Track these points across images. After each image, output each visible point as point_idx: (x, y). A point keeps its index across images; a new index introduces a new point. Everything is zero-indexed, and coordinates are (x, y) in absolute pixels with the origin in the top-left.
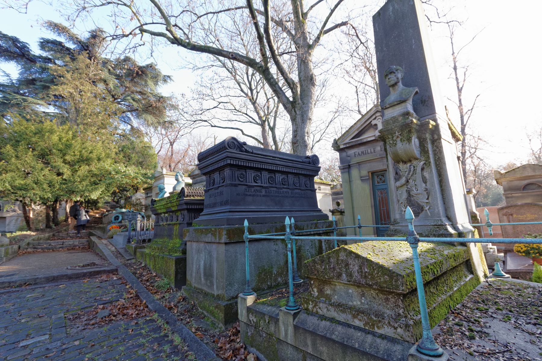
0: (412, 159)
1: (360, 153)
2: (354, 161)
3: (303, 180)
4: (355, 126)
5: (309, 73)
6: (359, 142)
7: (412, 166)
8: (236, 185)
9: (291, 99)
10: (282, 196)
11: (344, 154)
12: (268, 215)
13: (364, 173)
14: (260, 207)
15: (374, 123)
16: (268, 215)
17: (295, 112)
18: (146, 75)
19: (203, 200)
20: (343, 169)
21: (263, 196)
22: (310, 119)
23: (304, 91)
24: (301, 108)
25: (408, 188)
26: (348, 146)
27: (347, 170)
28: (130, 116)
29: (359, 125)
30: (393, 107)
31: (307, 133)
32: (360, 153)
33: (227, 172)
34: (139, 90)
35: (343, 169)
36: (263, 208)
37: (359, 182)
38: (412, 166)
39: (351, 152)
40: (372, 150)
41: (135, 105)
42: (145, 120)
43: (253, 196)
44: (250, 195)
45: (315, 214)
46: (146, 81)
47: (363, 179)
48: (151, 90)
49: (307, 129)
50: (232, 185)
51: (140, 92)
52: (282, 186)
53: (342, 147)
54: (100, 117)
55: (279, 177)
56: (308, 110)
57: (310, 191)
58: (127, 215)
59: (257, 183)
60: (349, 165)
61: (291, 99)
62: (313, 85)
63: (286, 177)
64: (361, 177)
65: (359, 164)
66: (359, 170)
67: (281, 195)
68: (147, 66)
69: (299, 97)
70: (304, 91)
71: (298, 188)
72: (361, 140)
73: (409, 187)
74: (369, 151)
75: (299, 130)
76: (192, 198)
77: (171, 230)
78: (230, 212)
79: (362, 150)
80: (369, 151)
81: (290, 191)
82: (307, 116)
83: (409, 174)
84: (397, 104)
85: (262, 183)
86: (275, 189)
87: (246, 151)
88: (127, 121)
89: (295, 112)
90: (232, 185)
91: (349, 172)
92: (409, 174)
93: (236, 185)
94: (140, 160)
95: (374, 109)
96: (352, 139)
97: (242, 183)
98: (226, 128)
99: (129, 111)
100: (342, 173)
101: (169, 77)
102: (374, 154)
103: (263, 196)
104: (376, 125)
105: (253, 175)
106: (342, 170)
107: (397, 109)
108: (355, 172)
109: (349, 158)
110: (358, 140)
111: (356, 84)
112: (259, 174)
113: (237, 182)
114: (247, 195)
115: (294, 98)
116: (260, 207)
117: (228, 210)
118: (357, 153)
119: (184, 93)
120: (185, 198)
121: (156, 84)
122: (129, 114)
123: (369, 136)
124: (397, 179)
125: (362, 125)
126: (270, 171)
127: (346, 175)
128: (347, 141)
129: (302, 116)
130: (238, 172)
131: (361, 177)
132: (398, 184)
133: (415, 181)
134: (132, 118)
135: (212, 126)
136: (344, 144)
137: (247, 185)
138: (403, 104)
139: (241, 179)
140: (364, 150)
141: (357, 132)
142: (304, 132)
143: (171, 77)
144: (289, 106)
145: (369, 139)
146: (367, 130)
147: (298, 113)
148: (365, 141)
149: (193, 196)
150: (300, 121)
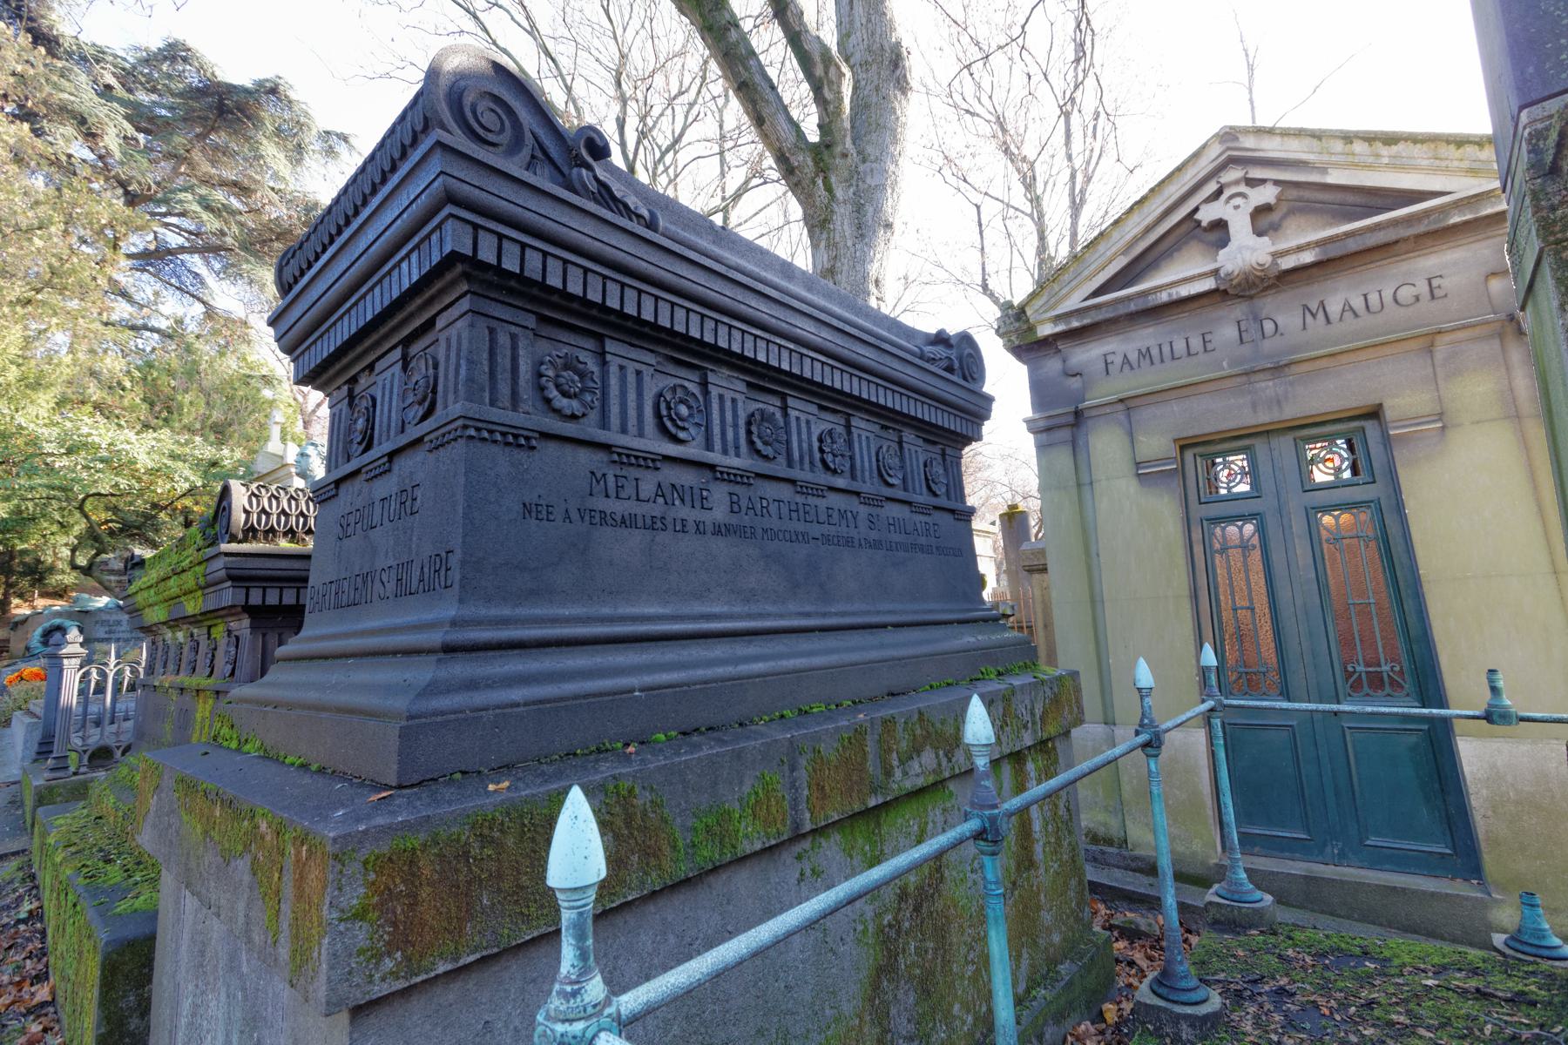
1: (1133, 357)
3: (917, 450)
4: (1116, 235)
5: (885, 35)
6: (1133, 307)
8: (518, 440)
9: (813, 136)
10: (827, 539)
11: (1053, 365)
12: (756, 660)
13: (1156, 444)
14: (698, 608)
16: (756, 660)
17: (829, 189)
18: (257, 122)
19: (307, 557)
20: (1048, 429)
21: (719, 530)
22: (889, 226)
23: (867, 106)
24: (854, 176)
26: (1075, 324)
27: (1065, 434)
28: (202, 270)
29: (1133, 228)
31: (877, 282)
32: (1133, 357)
33: (457, 328)
34: (230, 175)
35: (1048, 429)
36: (722, 611)
39: (1087, 354)
40: (1196, 343)
41: (212, 223)
42: (251, 282)
43: (654, 525)
44: (627, 522)
45: (970, 638)
46: (255, 149)
47: (1145, 473)
48: (276, 176)
49: (876, 265)
50: (480, 432)
51: (235, 184)
52: (824, 478)
53: (1046, 330)
54: (36, 241)
55: (808, 423)
56: (881, 187)
57: (948, 517)
58: (103, 623)
59: (676, 440)
60: (1078, 414)
61: (813, 136)
62: (903, 86)
63: (840, 429)
64: (1138, 465)
65: (1127, 404)
67: (816, 530)
68: (260, 84)
69: (847, 125)
70: (867, 106)
71: (900, 494)
74: (1180, 346)
75: (844, 265)
76: (284, 545)
77: (185, 719)
78: (450, 649)
79: (1143, 345)
80: (1180, 346)
81: (863, 511)
82: (878, 210)
85: (709, 446)
86: (785, 492)
87: (605, 194)
88: (191, 289)
89: (829, 189)
90: (480, 432)
93: (518, 440)
94: (217, 415)
95: (1215, 150)
96: (1097, 293)
97: (569, 429)
99: (192, 250)
101: (344, 138)
102: (1202, 357)
103: (719, 530)
104: (1220, 225)
105: (652, 386)
108: (1106, 444)
109: (1075, 383)
110: (1129, 298)
111: (978, 198)
112: (693, 388)
113: (531, 417)
114: (604, 518)
116: (698, 608)
117: (435, 638)
118: (1118, 360)
120: (225, 547)
121: (297, 153)
122: (195, 262)
123: (1185, 274)
125: (1149, 229)
126: (761, 377)
127: (1063, 458)
128: (1074, 302)
129: (859, 209)
130: (543, 347)
134: (210, 280)
136: (1058, 319)
137: (606, 447)
139: (561, 402)
141: (1122, 262)
142: (865, 278)
143: (351, 140)
144: (803, 160)
145: (1185, 291)
147: (839, 193)
148: (1164, 297)
149: (291, 533)
150: (848, 231)
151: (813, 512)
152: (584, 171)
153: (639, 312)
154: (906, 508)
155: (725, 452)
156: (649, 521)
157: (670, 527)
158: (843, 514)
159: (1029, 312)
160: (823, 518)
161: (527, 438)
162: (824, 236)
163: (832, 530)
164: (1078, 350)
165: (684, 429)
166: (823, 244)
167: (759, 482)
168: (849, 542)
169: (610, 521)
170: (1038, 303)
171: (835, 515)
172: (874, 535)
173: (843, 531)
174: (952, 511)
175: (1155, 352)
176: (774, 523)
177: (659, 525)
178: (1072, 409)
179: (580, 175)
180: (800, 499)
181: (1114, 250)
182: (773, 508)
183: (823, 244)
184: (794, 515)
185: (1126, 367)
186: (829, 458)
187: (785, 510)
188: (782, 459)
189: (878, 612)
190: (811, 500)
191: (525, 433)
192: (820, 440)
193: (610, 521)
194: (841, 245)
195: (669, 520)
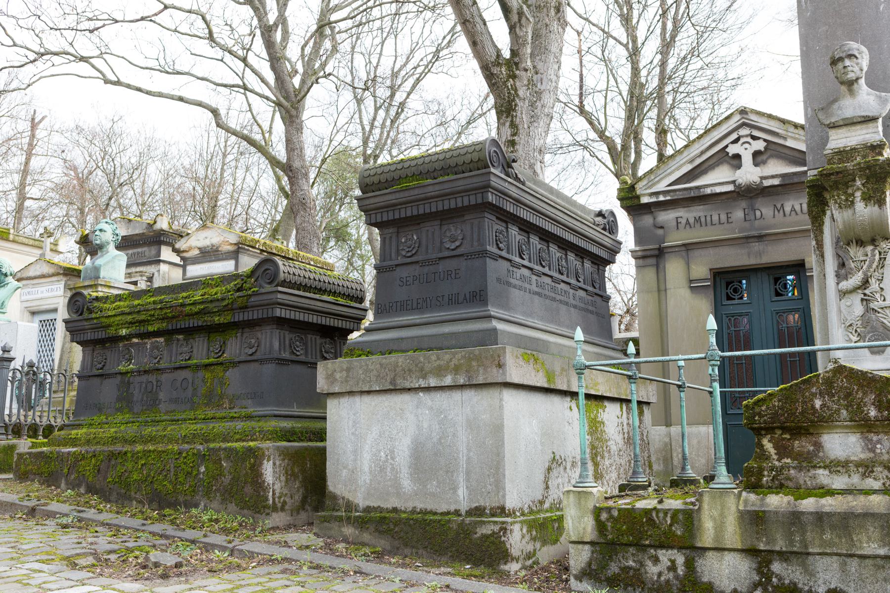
0: (878, 237)
1: (692, 221)
2: (674, 239)
7: (877, 251)
10: (561, 301)
11: (647, 220)
13: (701, 270)
15: (732, 150)
20: (644, 257)
25: (865, 295)
27: (653, 261)
30: (849, 128)
32: (692, 221)
37: (685, 292)
38: (877, 251)
39: (667, 217)
40: (723, 217)
47: (694, 287)
53: (645, 200)
64: (691, 281)
65: (688, 247)
66: (688, 264)
72: (698, 188)
73: (867, 292)
74: (715, 218)
79: (697, 214)
80: (715, 218)
83: (870, 266)
84: (859, 122)
91: (659, 268)
92: (870, 266)
98: (160, 95)
100: (638, 267)
102: (726, 226)
106: (641, 261)
107: (859, 132)
108: (674, 269)
110: (691, 189)
115: (514, 53)
118: (684, 221)
119: (828, 60)
124: (839, 277)
125: (702, 153)
127: (651, 273)
128: (662, 186)
131: (691, 281)
132: (845, 285)
133: (881, 280)
135: (107, 81)
138: (871, 125)
140: (702, 214)
141: (689, 167)
145: (718, 189)
146: (712, 167)
148: (708, 191)
158: (565, 292)
163: (562, 298)
164: (662, 213)
168: (567, 304)
172: (574, 302)
175: (703, 219)
176: (547, 293)
180: (553, 284)
190: (515, 269)
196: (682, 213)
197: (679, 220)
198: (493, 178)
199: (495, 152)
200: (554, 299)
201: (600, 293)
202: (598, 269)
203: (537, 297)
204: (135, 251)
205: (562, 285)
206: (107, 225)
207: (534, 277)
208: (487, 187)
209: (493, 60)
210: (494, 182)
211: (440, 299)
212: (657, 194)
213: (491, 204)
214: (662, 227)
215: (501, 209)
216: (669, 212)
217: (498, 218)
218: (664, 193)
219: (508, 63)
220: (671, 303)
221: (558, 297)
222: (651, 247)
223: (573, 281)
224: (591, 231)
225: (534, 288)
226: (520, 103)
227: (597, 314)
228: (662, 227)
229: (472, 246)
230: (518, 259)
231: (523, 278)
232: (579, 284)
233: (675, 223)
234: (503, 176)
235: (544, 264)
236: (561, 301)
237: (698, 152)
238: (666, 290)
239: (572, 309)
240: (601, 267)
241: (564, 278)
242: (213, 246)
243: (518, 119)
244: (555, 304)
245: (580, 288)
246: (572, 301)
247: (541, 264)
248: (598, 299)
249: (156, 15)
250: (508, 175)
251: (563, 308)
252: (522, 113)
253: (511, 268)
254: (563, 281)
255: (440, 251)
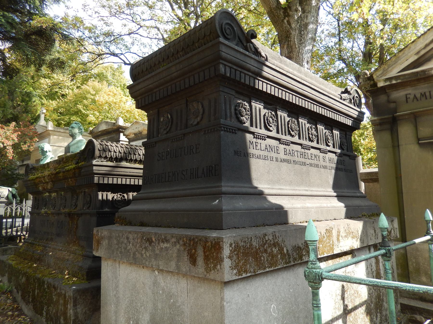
1: (418, 96)
10: (311, 165)
11: (383, 98)
32: (418, 96)
53: (381, 84)
64: (419, 139)
67: (308, 161)
79: (422, 91)
108: (405, 132)
118: (412, 97)
125: (427, 46)
127: (386, 136)
140: (426, 90)
147: (293, 26)
151: (307, 155)
152: (251, 45)
153: (240, 80)
154: (300, 147)
155: (256, 127)
156: (264, 157)
157: (269, 159)
158: (315, 156)
159: (375, 77)
160: (310, 157)
161: (235, 130)
162: (287, 43)
163: (313, 162)
164: (395, 92)
165: (271, 126)
166: (285, 47)
167: (268, 139)
168: (317, 166)
169: (255, 157)
170: (379, 73)
171: (313, 156)
172: (324, 164)
173: (315, 162)
174: (349, 156)
175: (428, 94)
176: (296, 159)
177: (266, 158)
178: (391, 116)
179: (250, 46)
180: (303, 150)
181: (411, 53)
182: (296, 153)
183: (285, 47)
184: (301, 156)
185: (415, 100)
186: (311, 136)
187: (299, 154)
188: (297, 137)
189: (327, 191)
190: (259, 141)
191: (229, 127)
192: (308, 130)
193: (255, 157)
194: (294, 47)
195: (269, 157)
196: (410, 91)
197: (408, 96)
198: (223, 48)
199: (228, 24)
200: (304, 164)
201: (348, 153)
202: (346, 135)
203: (285, 163)
204: (111, 136)
205: (312, 150)
206: (76, 125)
207: (282, 147)
208: (218, 58)
209: (274, 6)
210: (225, 52)
211: (185, 173)
212: (390, 79)
213: (224, 77)
214: (394, 102)
215: (239, 82)
216: (399, 91)
217: (237, 92)
218: (396, 78)
219: (285, 9)
220: (403, 155)
221: (308, 161)
222: (386, 117)
223: (323, 147)
224: (338, 104)
225: (282, 156)
226: (293, 33)
227: (346, 170)
228: (394, 102)
229: (210, 121)
230: (263, 131)
231: (269, 148)
232: (328, 148)
233: (405, 99)
234: (242, 50)
235: (293, 133)
236: (311, 165)
237: (422, 46)
238: (398, 146)
239: (322, 170)
240: (348, 133)
241: (314, 144)
242: (139, 131)
243: (292, 43)
244: (304, 168)
245: (330, 151)
246: (322, 163)
247: (290, 134)
248: (347, 159)
249: (137, 30)
250: (246, 49)
251: (314, 169)
252: (294, 39)
253: (255, 140)
254: (313, 148)
255: (186, 127)
